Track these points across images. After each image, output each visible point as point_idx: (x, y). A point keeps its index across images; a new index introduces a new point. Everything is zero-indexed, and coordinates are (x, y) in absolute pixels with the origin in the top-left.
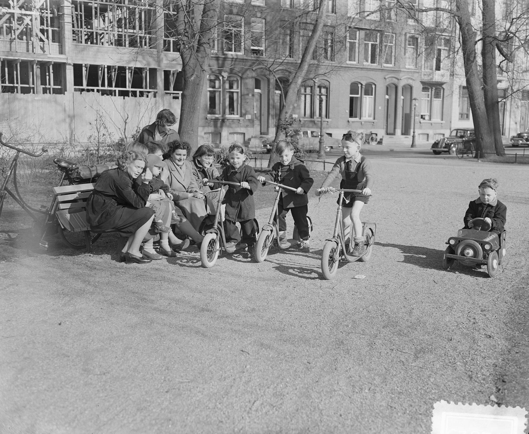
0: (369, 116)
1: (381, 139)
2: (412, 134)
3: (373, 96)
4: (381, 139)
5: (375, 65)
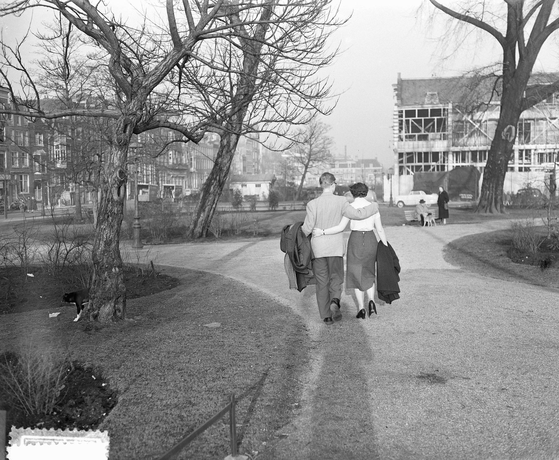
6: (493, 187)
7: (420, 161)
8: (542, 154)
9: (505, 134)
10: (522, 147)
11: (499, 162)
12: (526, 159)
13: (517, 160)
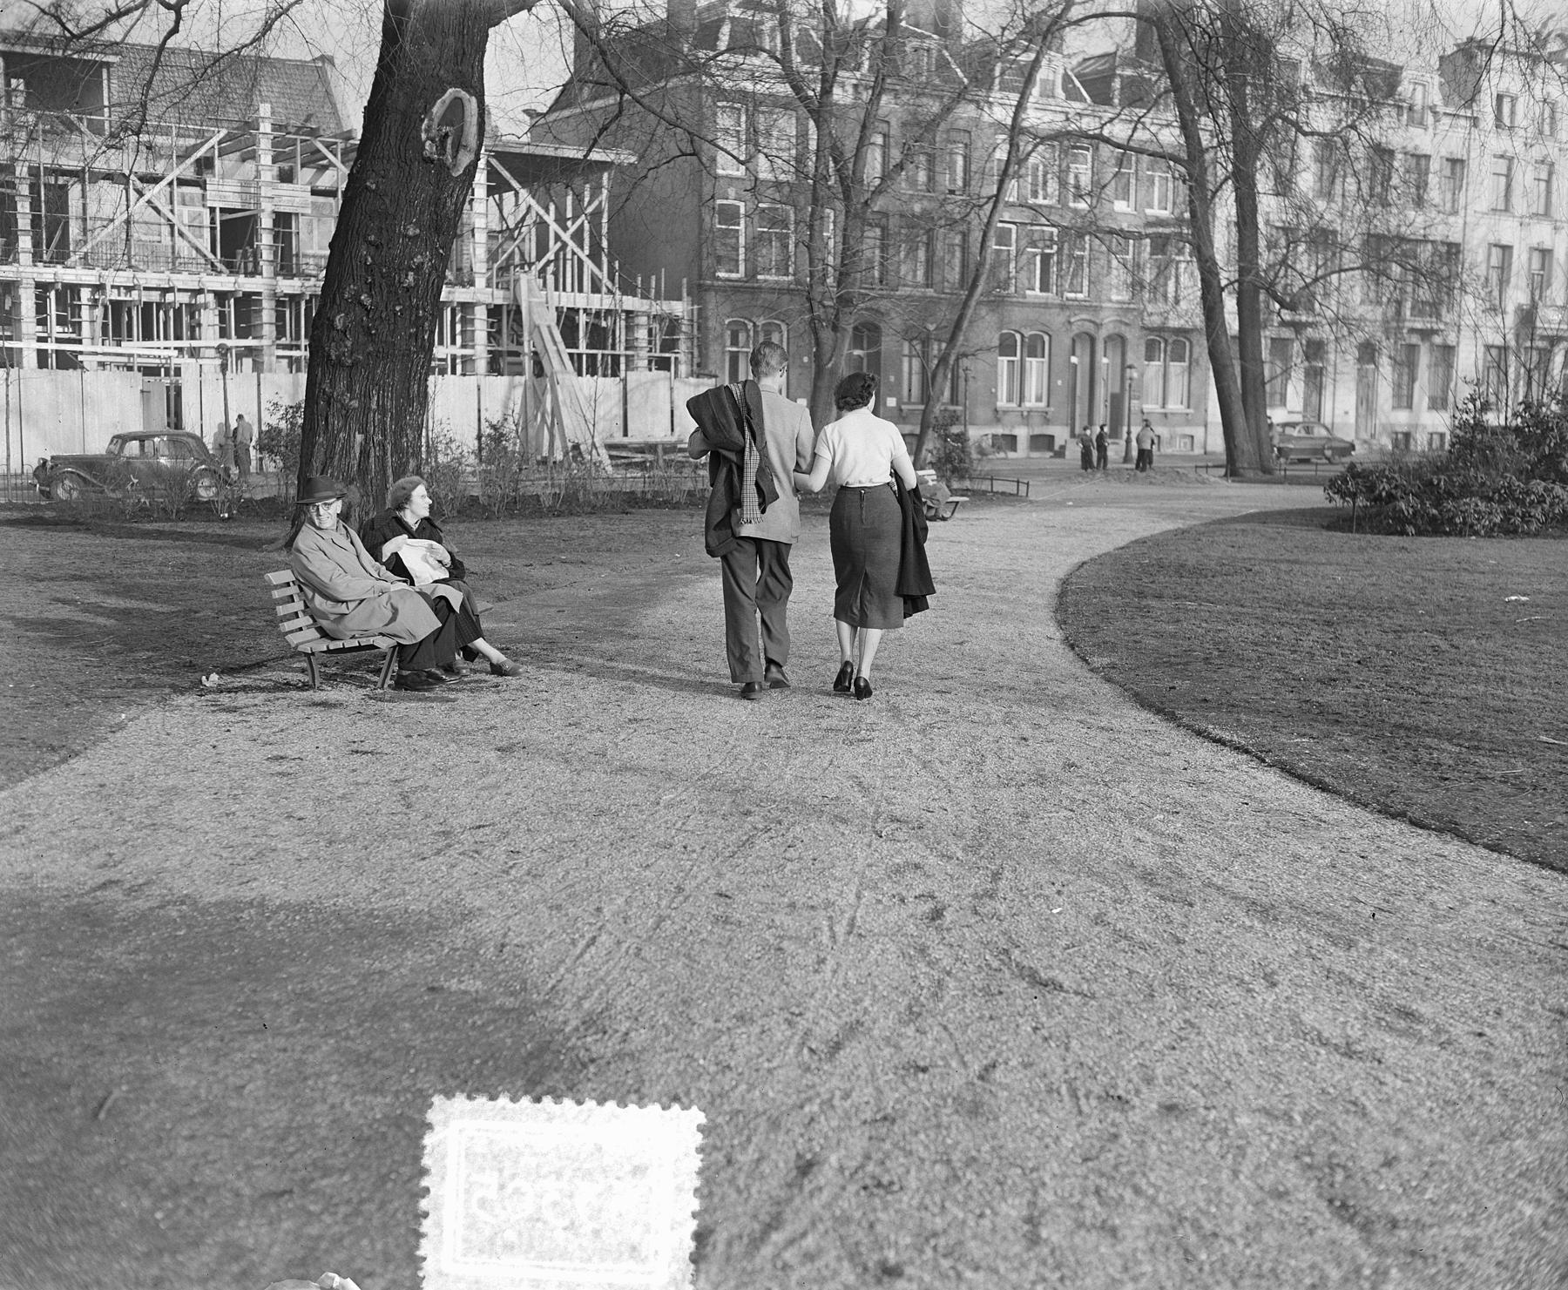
0: (1039, 399)
1: (1063, 448)
2: (1125, 436)
3: (1046, 359)
4: (1063, 448)
5: (1050, 296)
6: (382, 409)
8: (117, 306)
9: (434, 132)
10: (47, 274)
12: (61, 321)
13: (29, 324)
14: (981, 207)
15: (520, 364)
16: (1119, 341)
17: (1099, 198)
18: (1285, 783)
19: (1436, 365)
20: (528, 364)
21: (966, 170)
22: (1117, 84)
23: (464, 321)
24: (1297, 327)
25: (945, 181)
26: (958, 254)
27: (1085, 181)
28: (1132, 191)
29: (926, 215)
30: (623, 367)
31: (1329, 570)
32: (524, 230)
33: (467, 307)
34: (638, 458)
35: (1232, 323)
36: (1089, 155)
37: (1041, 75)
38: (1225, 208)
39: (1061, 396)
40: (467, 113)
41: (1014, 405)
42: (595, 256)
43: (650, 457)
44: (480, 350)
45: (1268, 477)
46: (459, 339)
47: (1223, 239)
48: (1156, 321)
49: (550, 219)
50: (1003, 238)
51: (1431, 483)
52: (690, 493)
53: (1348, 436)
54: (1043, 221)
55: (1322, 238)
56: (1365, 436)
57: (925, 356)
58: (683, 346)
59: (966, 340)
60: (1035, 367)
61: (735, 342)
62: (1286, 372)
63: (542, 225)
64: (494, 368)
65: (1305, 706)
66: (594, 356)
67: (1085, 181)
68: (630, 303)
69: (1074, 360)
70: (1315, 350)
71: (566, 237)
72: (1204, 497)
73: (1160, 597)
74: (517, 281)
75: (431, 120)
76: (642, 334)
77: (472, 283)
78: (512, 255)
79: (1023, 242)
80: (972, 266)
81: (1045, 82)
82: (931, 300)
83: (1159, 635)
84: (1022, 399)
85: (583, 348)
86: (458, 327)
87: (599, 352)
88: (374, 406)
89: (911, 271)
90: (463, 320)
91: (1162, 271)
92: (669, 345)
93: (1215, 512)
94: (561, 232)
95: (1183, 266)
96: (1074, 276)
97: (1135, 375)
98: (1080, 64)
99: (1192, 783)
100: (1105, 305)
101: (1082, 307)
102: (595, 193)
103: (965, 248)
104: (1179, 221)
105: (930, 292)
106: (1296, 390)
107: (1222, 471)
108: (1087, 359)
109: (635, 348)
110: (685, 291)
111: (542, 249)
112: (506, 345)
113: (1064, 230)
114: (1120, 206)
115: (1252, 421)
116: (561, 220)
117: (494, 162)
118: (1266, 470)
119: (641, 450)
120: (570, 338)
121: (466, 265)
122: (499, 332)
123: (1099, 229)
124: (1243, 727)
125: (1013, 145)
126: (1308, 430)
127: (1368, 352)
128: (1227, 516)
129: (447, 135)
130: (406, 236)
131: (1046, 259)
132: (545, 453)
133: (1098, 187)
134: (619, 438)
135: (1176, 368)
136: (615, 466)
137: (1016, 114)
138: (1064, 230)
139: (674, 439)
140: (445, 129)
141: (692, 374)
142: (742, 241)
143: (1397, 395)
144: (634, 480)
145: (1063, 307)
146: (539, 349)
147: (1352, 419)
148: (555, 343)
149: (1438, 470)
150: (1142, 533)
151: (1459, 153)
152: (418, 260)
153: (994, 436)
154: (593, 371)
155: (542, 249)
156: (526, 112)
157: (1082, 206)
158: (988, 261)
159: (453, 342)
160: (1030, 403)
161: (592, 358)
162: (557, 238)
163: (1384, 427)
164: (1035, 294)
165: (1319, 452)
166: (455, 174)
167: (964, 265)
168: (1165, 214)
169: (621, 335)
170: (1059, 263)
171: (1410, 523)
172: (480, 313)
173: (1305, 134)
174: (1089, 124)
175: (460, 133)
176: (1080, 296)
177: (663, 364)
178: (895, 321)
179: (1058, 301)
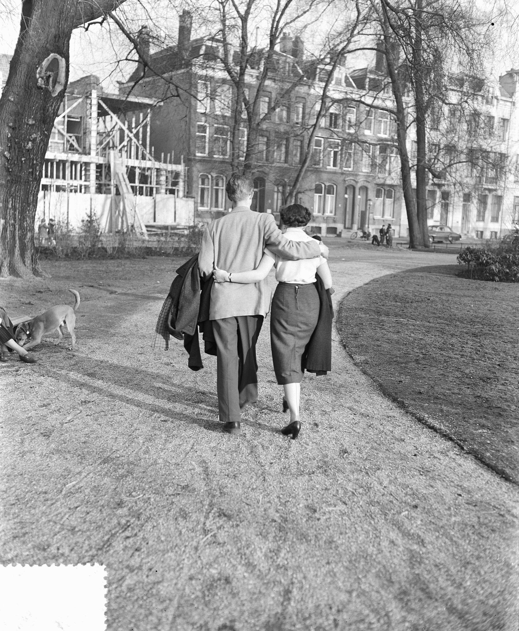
0: (331, 212)
1: (340, 233)
3: (334, 195)
4: (340, 233)
6: (14, 208)
7: (141, 188)
9: (43, 74)
11: (30, 144)
14: (309, 129)
15: (110, 189)
16: (365, 189)
17: (359, 127)
18: (481, 471)
19: (495, 204)
20: (113, 190)
21: (304, 113)
22: (368, 80)
23: (86, 170)
24: (439, 186)
25: (294, 118)
26: (299, 150)
27: (353, 120)
28: (372, 125)
29: (286, 133)
30: (154, 192)
31: (466, 300)
32: (114, 132)
33: (87, 164)
34: (159, 231)
35: (414, 183)
36: (355, 110)
37: (336, 74)
38: (412, 134)
39: (340, 212)
40: (60, 66)
41: (320, 214)
42: (144, 145)
43: (164, 231)
44: (93, 183)
45: (427, 249)
46: (83, 178)
47: (410, 146)
48: (381, 181)
49: (125, 128)
50: (318, 143)
51: (506, 257)
52: (176, 249)
53: (458, 232)
54: (336, 137)
55: (451, 149)
56: (465, 232)
57: (283, 193)
58: (181, 184)
59: (301, 186)
60: (330, 199)
61: (203, 183)
62: (434, 205)
63: (122, 131)
64: (99, 190)
65: (479, 401)
66: (142, 187)
67: (353, 120)
68: (157, 165)
69: (346, 196)
70: (446, 196)
71: (131, 135)
72: (402, 258)
73: (388, 315)
74: (109, 154)
75: (41, 68)
76: (163, 178)
77: (89, 154)
78: (109, 142)
79: (327, 145)
80: (304, 155)
81: (337, 78)
82: (286, 168)
83: (389, 341)
84: (324, 212)
85: (137, 184)
86: (83, 173)
87: (144, 186)
88: (10, 206)
89: (279, 155)
90: (85, 170)
91: (384, 160)
92: (175, 184)
93: (407, 266)
94: (129, 134)
95: (392, 159)
96: (347, 160)
97: (371, 203)
98: (352, 72)
99: (424, 471)
100: (360, 173)
101: (350, 174)
102: (145, 118)
103: (302, 147)
104: (392, 140)
105: (286, 165)
106: (437, 212)
107: (408, 246)
108: (352, 196)
109: (160, 185)
110: (182, 161)
111: (122, 140)
112: (103, 182)
113: (344, 140)
114: (367, 132)
115: (421, 225)
116: (130, 129)
117: (101, 101)
118: (426, 246)
119: (160, 228)
120: (132, 179)
121: (87, 146)
122: (101, 175)
123: (359, 141)
124: (445, 416)
125: (323, 103)
126: (441, 229)
127: (467, 198)
128: (413, 267)
129: (49, 76)
130: (28, 124)
131: (335, 153)
132: (119, 228)
133: (358, 124)
134: (152, 223)
135: (389, 201)
136: (149, 235)
137: (324, 91)
138: (344, 140)
139: (174, 224)
140: (49, 73)
141: (184, 196)
142: (207, 140)
143: (479, 215)
144: (153, 243)
145: (342, 174)
146: (118, 183)
147: (460, 224)
148: (125, 181)
149: (508, 251)
150: (376, 276)
151: (507, 117)
152: (34, 136)
153: (312, 227)
154: (141, 194)
155: (122, 140)
156: (118, 82)
157: (352, 131)
158: (311, 152)
159: (81, 179)
160: (328, 214)
161: (141, 188)
162: (128, 136)
163: (474, 228)
164: (331, 167)
165: (446, 238)
166: (54, 95)
167: (301, 154)
168: (386, 136)
169: (154, 179)
170: (341, 154)
171: (497, 276)
172: (93, 167)
173: (446, 104)
174: (356, 97)
175: (57, 75)
176: (350, 169)
177: (172, 192)
178: (272, 177)
179: (340, 171)
